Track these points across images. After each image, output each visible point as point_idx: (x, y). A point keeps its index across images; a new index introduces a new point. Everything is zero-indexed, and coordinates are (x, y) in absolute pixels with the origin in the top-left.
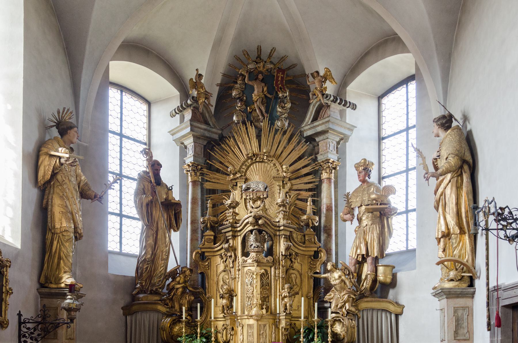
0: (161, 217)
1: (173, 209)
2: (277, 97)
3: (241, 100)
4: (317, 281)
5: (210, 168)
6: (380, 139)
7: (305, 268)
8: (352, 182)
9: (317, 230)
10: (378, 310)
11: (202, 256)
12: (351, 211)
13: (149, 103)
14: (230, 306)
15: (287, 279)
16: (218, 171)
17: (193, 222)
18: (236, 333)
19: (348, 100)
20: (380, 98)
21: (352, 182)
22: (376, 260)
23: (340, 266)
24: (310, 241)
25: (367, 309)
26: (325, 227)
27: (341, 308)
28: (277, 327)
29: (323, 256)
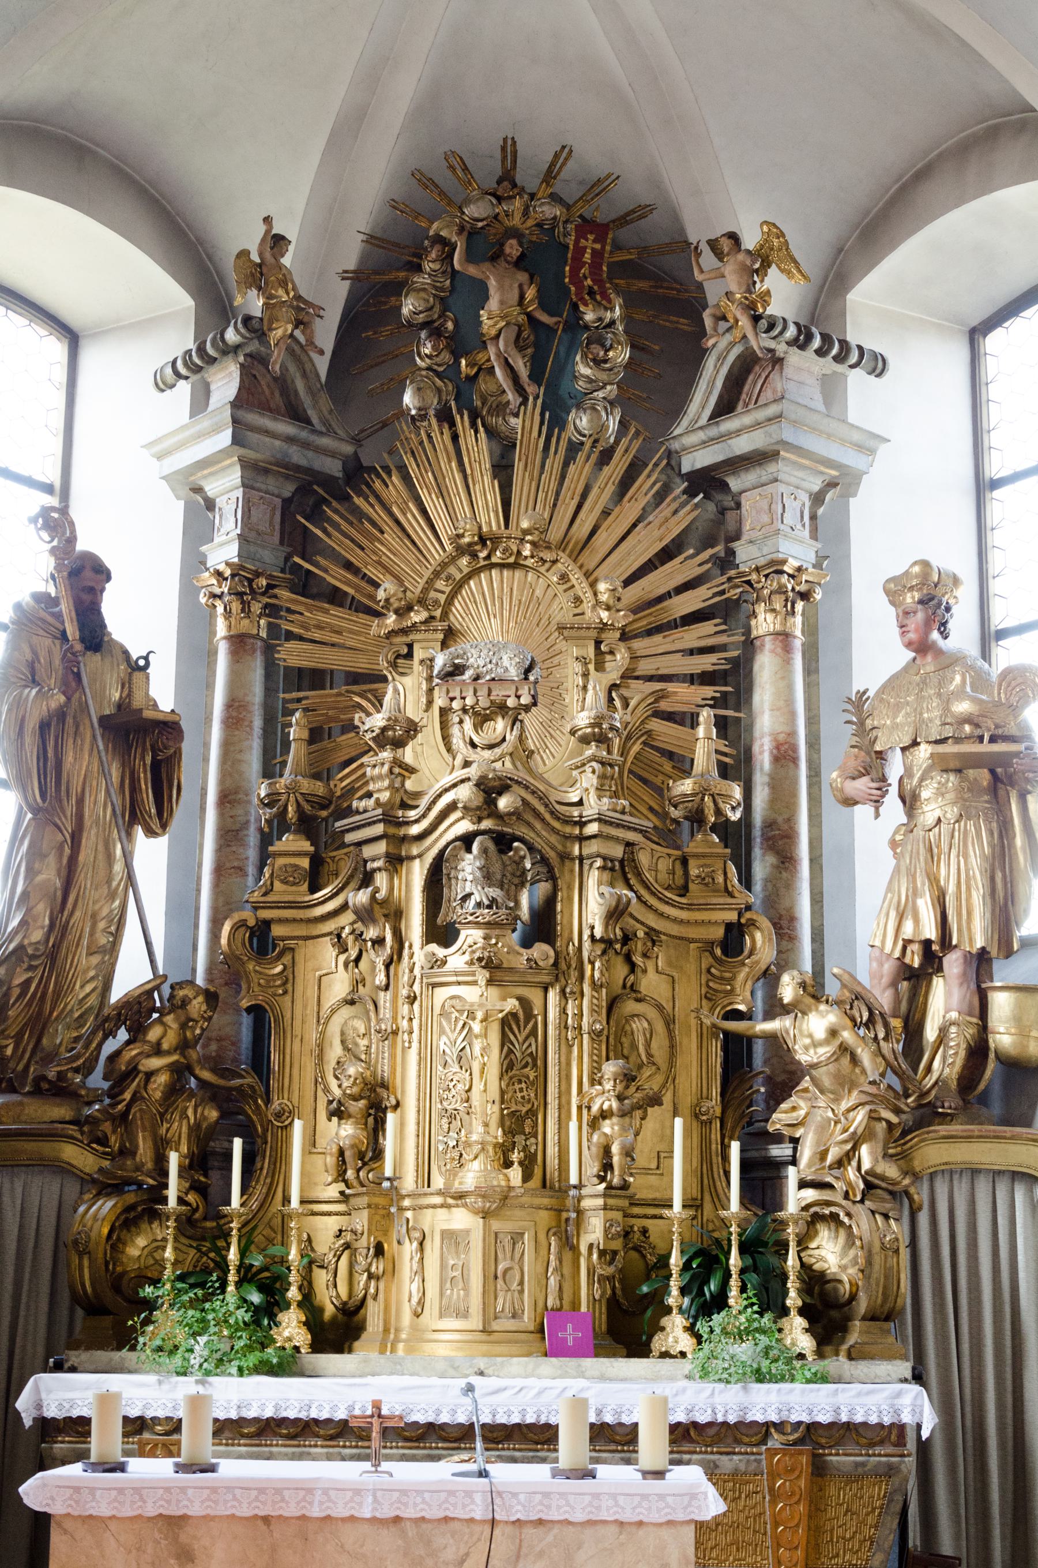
0: (95, 773)
1: (146, 751)
2: (575, 325)
3: (436, 333)
4: (736, 1051)
6: (984, 487)
7: (688, 995)
8: (876, 649)
9: (736, 837)
10: (997, 1174)
11: (260, 940)
12: (872, 764)
13: (72, 339)
15: (613, 1041)
16: (335, 597)
18: (393, 1270)
21: (876, 649)
23: (832, 988)
24: (707, 882)
25: (951, 1172)
26: (769, 825)
27: (840, 1163)
28: (568, 1244)
29: (762, 943)
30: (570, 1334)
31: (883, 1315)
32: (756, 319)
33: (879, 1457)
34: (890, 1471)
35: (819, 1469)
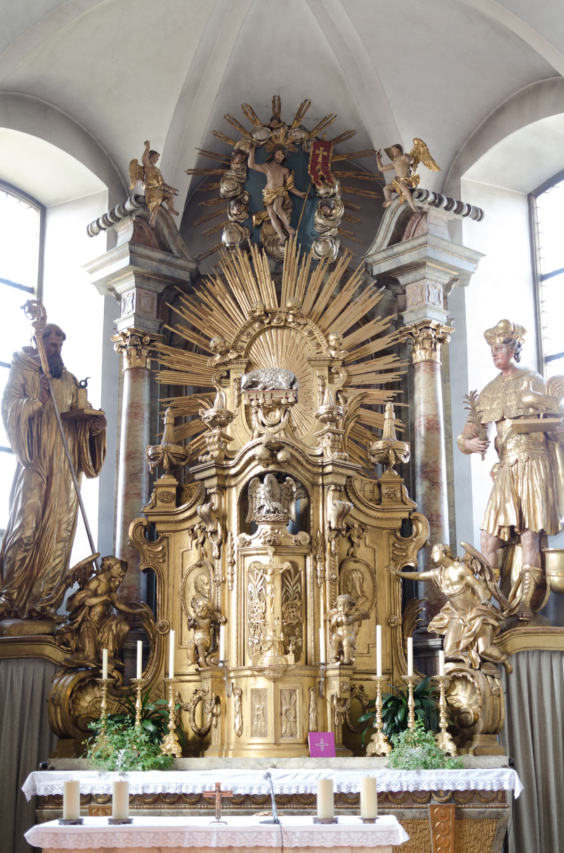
0: (60, 445)
1: (86, 431)
2: (314, 196)
3: (239, 202)
4: (409, 588)
5: (171, 340)
6: (537, 279)
8: (481, 369)
9: (407, 472)
10: (552, 653)
11: (150, 533)
12: (480, 432)
13: (43, 209)
14: (213, 648)
15: (342, 584)
16: (187, 346)
17: (130, 457)
18: (225, 711)
19: (464, 200)
20: (531, 197)
21: (481, 369)
22: (541, 538)
23: (461, 553)
25: (527, 652)
26: (425, 465)
28: (321, 696)
29: (422, 529)
30: (322, 745)
31: (492, 731)
32: (412, 191)
33: (492, 809)
34: (498, 816)
35: (459, 816)
